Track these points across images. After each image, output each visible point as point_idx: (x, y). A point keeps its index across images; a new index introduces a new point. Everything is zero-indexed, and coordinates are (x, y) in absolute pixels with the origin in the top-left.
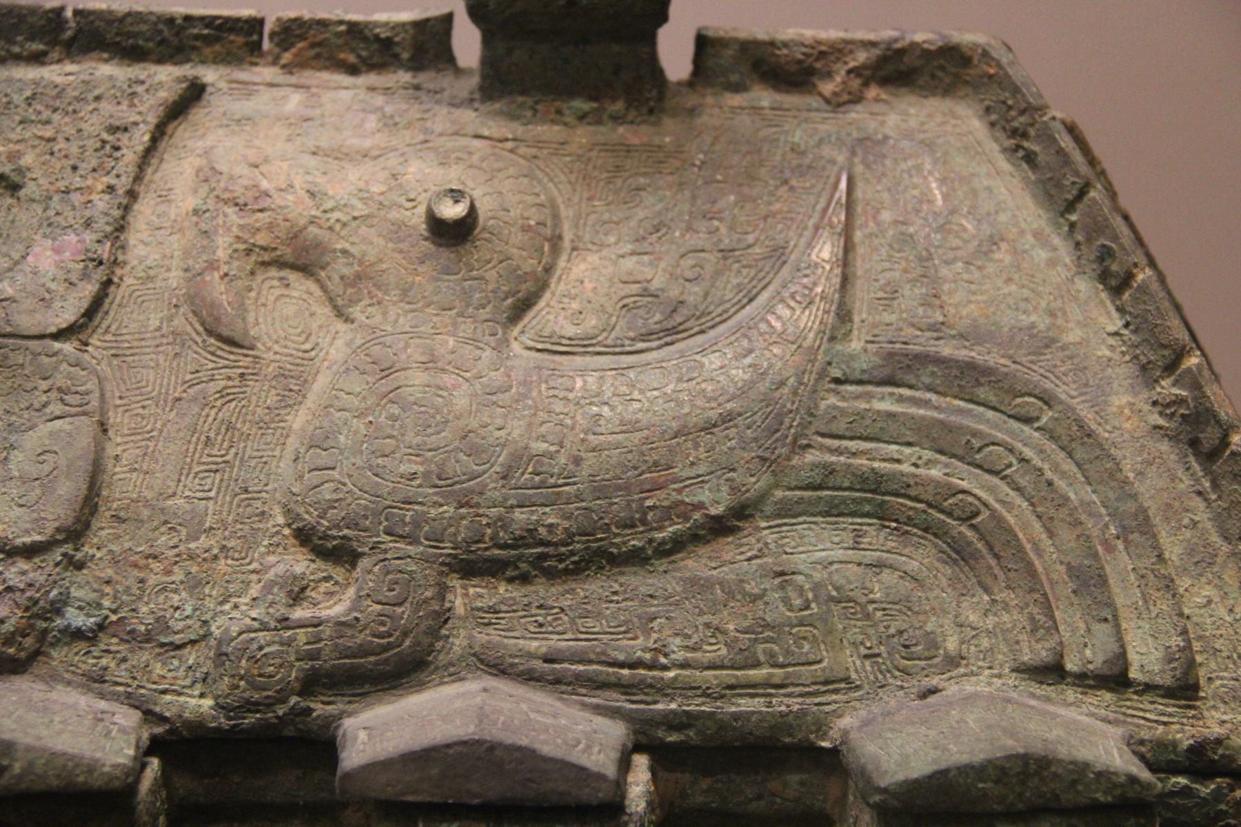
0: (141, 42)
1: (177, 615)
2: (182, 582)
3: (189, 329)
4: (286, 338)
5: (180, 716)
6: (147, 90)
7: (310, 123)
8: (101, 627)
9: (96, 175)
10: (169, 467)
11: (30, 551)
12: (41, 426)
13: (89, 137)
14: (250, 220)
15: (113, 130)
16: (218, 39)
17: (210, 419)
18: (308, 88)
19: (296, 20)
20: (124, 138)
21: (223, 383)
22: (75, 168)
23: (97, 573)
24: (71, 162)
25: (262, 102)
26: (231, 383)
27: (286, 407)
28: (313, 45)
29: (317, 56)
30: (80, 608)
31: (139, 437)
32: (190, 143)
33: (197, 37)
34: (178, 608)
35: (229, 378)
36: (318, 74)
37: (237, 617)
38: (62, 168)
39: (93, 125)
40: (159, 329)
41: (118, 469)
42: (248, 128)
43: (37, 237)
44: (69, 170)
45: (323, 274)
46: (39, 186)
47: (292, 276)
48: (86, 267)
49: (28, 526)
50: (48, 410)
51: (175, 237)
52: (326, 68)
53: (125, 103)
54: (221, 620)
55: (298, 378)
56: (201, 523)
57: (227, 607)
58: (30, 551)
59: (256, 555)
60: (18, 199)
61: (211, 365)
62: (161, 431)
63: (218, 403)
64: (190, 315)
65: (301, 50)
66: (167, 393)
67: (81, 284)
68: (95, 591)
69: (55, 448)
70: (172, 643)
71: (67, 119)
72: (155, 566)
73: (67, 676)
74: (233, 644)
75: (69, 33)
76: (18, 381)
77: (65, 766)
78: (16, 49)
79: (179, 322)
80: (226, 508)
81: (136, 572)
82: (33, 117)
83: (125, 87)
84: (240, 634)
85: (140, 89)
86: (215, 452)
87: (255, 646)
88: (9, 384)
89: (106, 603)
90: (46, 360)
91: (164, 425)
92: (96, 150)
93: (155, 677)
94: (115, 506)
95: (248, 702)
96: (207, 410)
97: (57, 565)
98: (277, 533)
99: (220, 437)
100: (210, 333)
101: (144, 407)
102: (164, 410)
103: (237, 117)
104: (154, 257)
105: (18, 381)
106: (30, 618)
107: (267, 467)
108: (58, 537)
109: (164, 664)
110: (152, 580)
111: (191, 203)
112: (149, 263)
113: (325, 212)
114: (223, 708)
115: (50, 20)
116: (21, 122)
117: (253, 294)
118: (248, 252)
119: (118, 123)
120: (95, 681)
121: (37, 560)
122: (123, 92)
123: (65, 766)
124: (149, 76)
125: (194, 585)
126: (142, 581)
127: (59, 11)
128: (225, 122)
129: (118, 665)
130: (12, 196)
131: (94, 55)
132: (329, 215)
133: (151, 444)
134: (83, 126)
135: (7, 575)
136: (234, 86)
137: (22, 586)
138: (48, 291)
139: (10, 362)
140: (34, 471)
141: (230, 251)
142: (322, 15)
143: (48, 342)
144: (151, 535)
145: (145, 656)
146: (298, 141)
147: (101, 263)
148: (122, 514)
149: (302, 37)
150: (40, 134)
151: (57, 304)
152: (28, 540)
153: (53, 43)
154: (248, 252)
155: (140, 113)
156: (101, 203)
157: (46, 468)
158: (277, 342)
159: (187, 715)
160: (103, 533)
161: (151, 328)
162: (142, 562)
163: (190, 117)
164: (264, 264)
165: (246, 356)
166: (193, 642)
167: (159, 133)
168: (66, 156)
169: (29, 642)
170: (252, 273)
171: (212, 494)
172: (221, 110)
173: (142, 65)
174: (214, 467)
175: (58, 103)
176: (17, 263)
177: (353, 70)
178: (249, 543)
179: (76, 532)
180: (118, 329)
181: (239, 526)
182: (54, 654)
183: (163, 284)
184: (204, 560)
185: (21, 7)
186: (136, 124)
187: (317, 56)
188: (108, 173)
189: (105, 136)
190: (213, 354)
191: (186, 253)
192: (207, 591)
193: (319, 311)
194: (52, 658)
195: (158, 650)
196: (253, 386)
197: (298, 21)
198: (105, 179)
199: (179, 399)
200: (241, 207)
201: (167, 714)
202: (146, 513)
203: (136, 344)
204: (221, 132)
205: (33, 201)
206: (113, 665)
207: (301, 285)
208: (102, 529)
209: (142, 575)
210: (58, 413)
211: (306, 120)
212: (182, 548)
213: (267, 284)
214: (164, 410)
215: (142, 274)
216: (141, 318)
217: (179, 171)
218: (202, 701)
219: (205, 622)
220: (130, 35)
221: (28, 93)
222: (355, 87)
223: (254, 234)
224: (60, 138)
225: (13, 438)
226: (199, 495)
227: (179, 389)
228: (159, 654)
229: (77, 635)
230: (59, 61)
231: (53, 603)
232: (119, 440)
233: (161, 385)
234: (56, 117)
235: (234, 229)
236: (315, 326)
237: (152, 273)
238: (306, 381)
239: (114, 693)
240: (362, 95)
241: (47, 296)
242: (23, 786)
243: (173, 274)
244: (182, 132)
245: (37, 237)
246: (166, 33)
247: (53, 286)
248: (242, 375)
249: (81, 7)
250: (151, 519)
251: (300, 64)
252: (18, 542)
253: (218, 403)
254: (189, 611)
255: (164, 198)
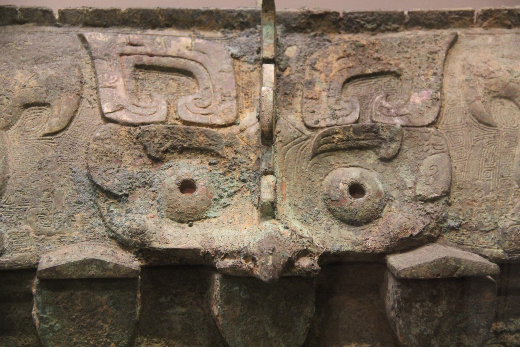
0: (433, 22)
1: (485, 221)
2: (486, 209)
3: (472, 121)
4: (507, 123)
5: (492, 256)
6: (441, 39)
7: (498, 47)
8: (460, 226)
9: (428, 69)
10: (474, 170)
11: (433, 200)
12: (428, 157)
13: (423, 56)
14: (488, 82)
15: (431, 53)
16: (460, 19)
17: (486, 152)
18: (494, 34)
19: (488, 10)
20: (436, 56)
21: (488, 140)
22: (420, 67)
23: (456, 207)
24: (418, 66)
25: (478, 40)
26: (491, 139)
27: (512, 147)
28: (495, 19)
29: (497, 23)
30: (452, 219)
31: (462, 160)
32: (457, 56)
33: (453, 19)
34: (485, 218)
35: (490, 138)
36: (497, 29)
37: (507, 222)
38: (415, 68)
39: (423, 52)
40: (461, 122)
41: (456, 171)
42: (476, 50)
43: (412, 92)
44: (418, 68)
45: (517, 99)
46: (408, 74)
47: (505, 101)
48: (433, 102)
49: (432, 191)
50: (429, 152)
51: (459, 90)
52: (499, 27)
53: (434, 43)
54: (501, 222)
55: (514, 137)
56: (489, 188)
57: (503, 217)
58: (433, 200)
59: (510, 199)
60: (401, 80)
61: (482, 134)
62: (469, 157)
63: (488, 146)
64: (472, 117)
65: (491, 21)
66: (469, 144)
67: (433, 108)
68: (457, 213)
69: (436, 164)
70: (485, 231)
71: (413, 50)
72: (475, 204)
73: (450, 243)
74: (508, 230)
75: (407, 20)
76: (417, 142)
77: (478, 266)
78: (389, 27)
79: (468, 119)
80: (497, 183)
81: (469, 207)
82: (401, 50)
83: (433, 38)
84: (510, 226)
85: (438, 38)
86: (489, 163)
87: (516, 230)
88: (414, 143)
89: (461, 217)
90: (426, 134)
91: (470, 155)
92: (427, 61)
93: (481, 243)
94: (458, 184)
95: (516, 250)
96: (484, 149)
97: (443, 204)
98: (517, 191)
99: (490, 159)
100: (480, 122)
101: (461, 149)
102: (469, 150)
103: (472, 46)
104: (454, 97)
105: (417, 142)
106: (437, 223)
107: (508, 168)
108: (443, 195)
109: (483, 238)
110: (475, 209)
111: (463, 77)
112: (452, 99)
113: (515, 77)
114: (507, 252)
115: (401, 16)
116: (398, 52)
117: (492, 108)
118: (489, 93)
119: (433, 51)
120: (461, 244)
121: (436, 203)
122: (432, 39)
123: (478, 266)
124: (441, 33)
125: (490, 210)
126: (471, 209)
127: (402, 13)
128: (468, 48)
129: (467, 239)
130: (398, 79)
131: (417, 27)
132: (517, 78)
133: (467, 162)
134: (420, 52)
135: (426, 209)
136: (468, 35)
137: (433, 212)
138: (421, 110)
139: (413, 136)
140: (430, 172)
141: (483, 93)
142: (498, 8)
143: (425, 128)
144: (472, 193)
145: (476, 236)
146: (496, 53)
147: (438, 100)
148: (461, 186)
149: (491, 16)
150: (405, 56)
151: (426, 115)
152: (432, 196)
153: (401, 24)
154: (489, 93)
155: (440, 47)
156: (432, 79)
157: (434, 171)
158: (504, 124)
159: (494, 255)
160: (455, 193)
161: (458, 122)
162: (471, 203)
163: (455, 47)
164: (494, 97)
165: (494, 130)
166: (492, 230)
167: (447, 53)
168: (416, 64)
169: (437, 231)
170: (491, 100)
171: (491, 178)
172: (466, 44)
173: (433, 30)
174: (490, 169)
175: (409, 45)
176: (407, 102)
177: (509, 27)
178: (507, 193)
179: (447, 193)
180: (447, 122)
181: (502, 189)
182: (445, 235)
183: (459, 106)
184: (492, 201)
185: (390, 12)
186: (439, 50)
187: (497, 23)
188: (433, 68)
189: (428, 55)
190: (482, 129)
191: (466, 95)
192: (495, 212)
193: (517, 113)
194: (443, 237)
195: (480, 233)
196: (499, 141)
197: (490, 11)
198: (432, 71)
199: (473, 146)
200: (485, 78)
201: (487, 255)
202: (469, 186)
203: (454, 127)
204: (467, 52)
205: (407, 80)
206: (465, 239)
207: (508, 104)
208: (455, 193)
209: (471, 207)
210: (433, 152)
211: (497, 46)
212: (484, 197)
213: (497, 104)
214: (469, 150)
215: (451, 103)
216: (454, 118)
217: (456, 65)
218: (498, 250)
219: (496, 223)
220: (429, 19)
221: (398, 42)
222: (511, 33)
223: (490, 87)
224: (412, 57)
225: (418, 162)
226: (487, 179)
227: (473, 142)
228: (481, 235)
229: (453, 229)
230: (403, 30)
231: (443, 217)
232: (455, 161)
233: (466, 141)
234: (409, 50)
235: (483, 85)
236: (516, 118)
237: (455, 102)
238: (517, 137)
239: (468, 249)
240: (514, 36)
241: (421, 112)
242: (464, 274)
243: (462, 102)
244: (453, 52)
245: (412, 92)
246: (442, 18)
247: (422, 109)
248: (494, 136)
249: (411, 10)
250: (471, 188)
251: (490, 26)
252: (429, 197)
253: (488, 146)
254: (489, 219)
255: (452, 76)
